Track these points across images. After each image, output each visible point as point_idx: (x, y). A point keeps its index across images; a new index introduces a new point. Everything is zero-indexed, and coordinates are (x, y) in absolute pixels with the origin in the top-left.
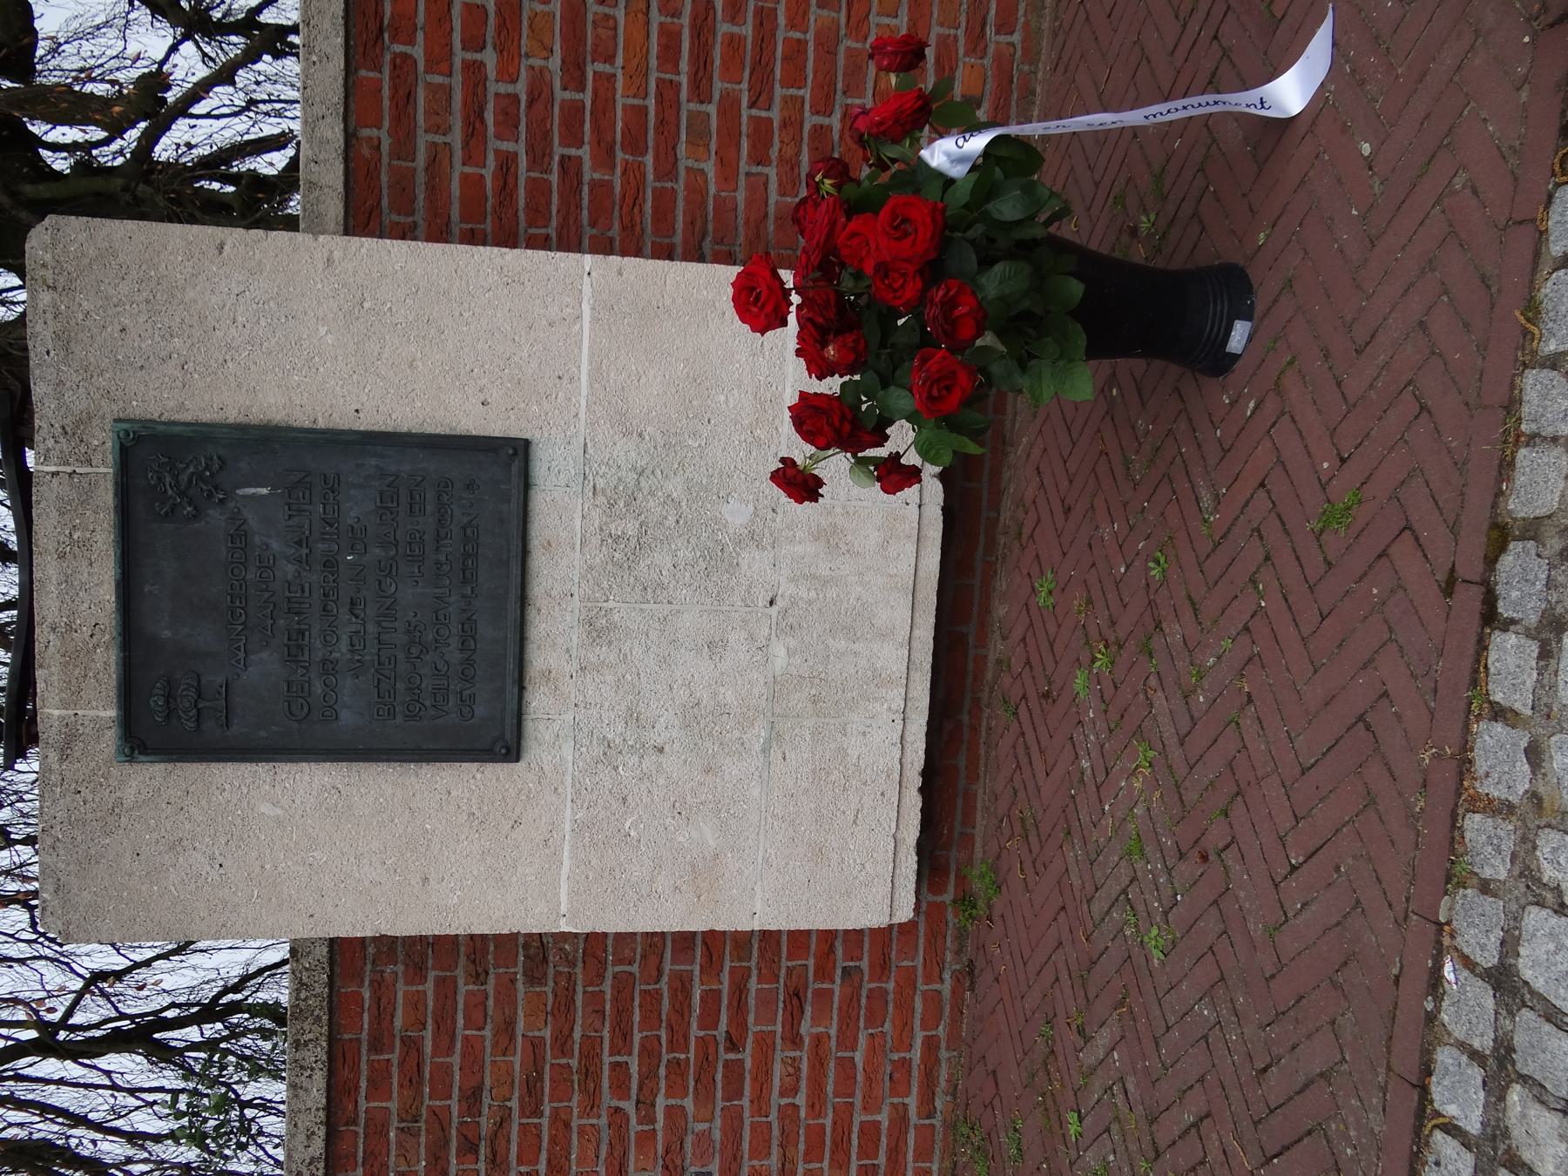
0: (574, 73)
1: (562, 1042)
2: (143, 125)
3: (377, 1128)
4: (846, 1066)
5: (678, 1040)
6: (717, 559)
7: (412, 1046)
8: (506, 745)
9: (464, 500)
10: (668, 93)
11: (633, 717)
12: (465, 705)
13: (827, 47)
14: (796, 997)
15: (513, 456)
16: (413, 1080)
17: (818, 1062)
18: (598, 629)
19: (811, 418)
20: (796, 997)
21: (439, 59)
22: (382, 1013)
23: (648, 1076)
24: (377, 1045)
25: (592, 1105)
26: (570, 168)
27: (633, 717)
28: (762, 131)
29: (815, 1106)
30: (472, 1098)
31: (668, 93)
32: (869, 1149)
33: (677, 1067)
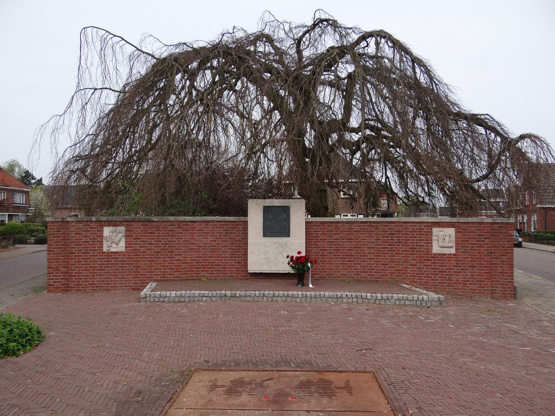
0: (321, 239)
1: (236, 241)
2: (373, 134)
3: (228, 225)
4: (232, 268)
5: (235, 252)
6: (281, 253)
7: (236, 228)
8: (265, 235)
9: (285, 231)
10: (320, 247)
11: (267, 246)
12: (268, 232)
13: (325, 261)
14: (239, 263)
15: (288, 235)
16: (233, 228)
17: (233, 265)
18: (274, 243)
19: (292, 257)
20: (239, 263)
21: (321, 229)
22: (239, 225)
23: (232, 249)
24: (236, 225)
25: (230, 244)
26: (313, 239)
27: (267, 246)
28: (318, 256)
29: (229, 265)
30: (231, 233)
31: (320, 247)
32: (224, 271)
33: (233, 252)
